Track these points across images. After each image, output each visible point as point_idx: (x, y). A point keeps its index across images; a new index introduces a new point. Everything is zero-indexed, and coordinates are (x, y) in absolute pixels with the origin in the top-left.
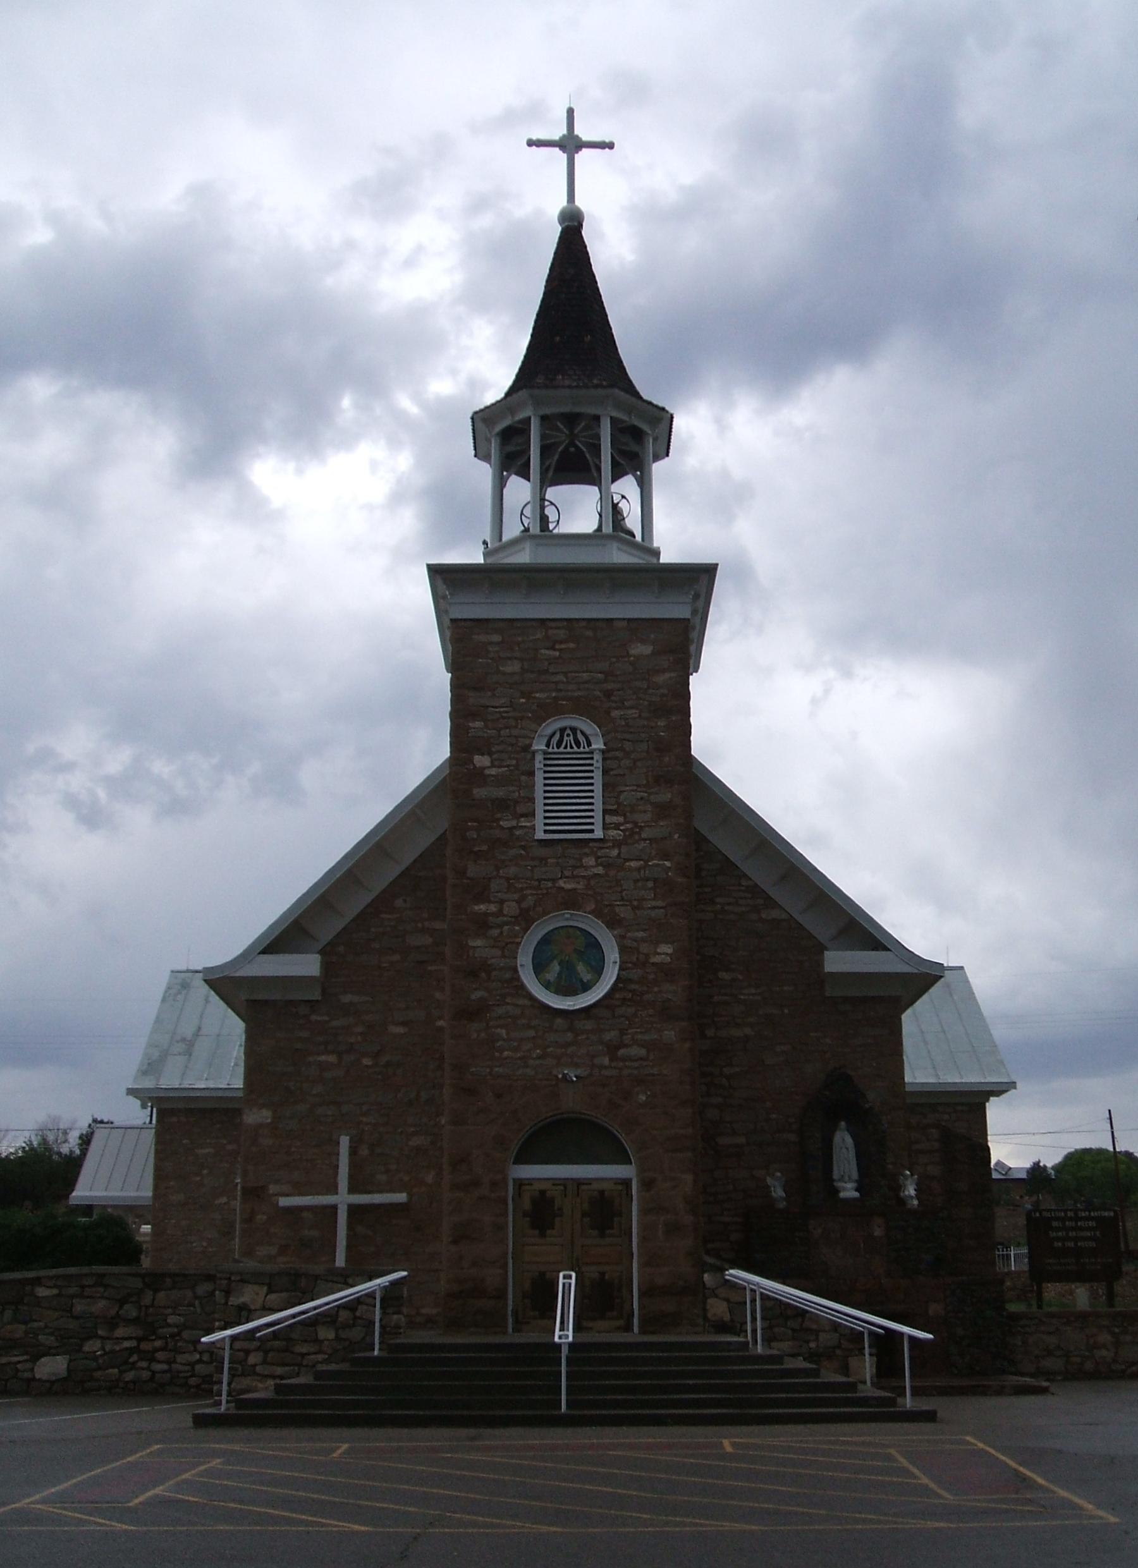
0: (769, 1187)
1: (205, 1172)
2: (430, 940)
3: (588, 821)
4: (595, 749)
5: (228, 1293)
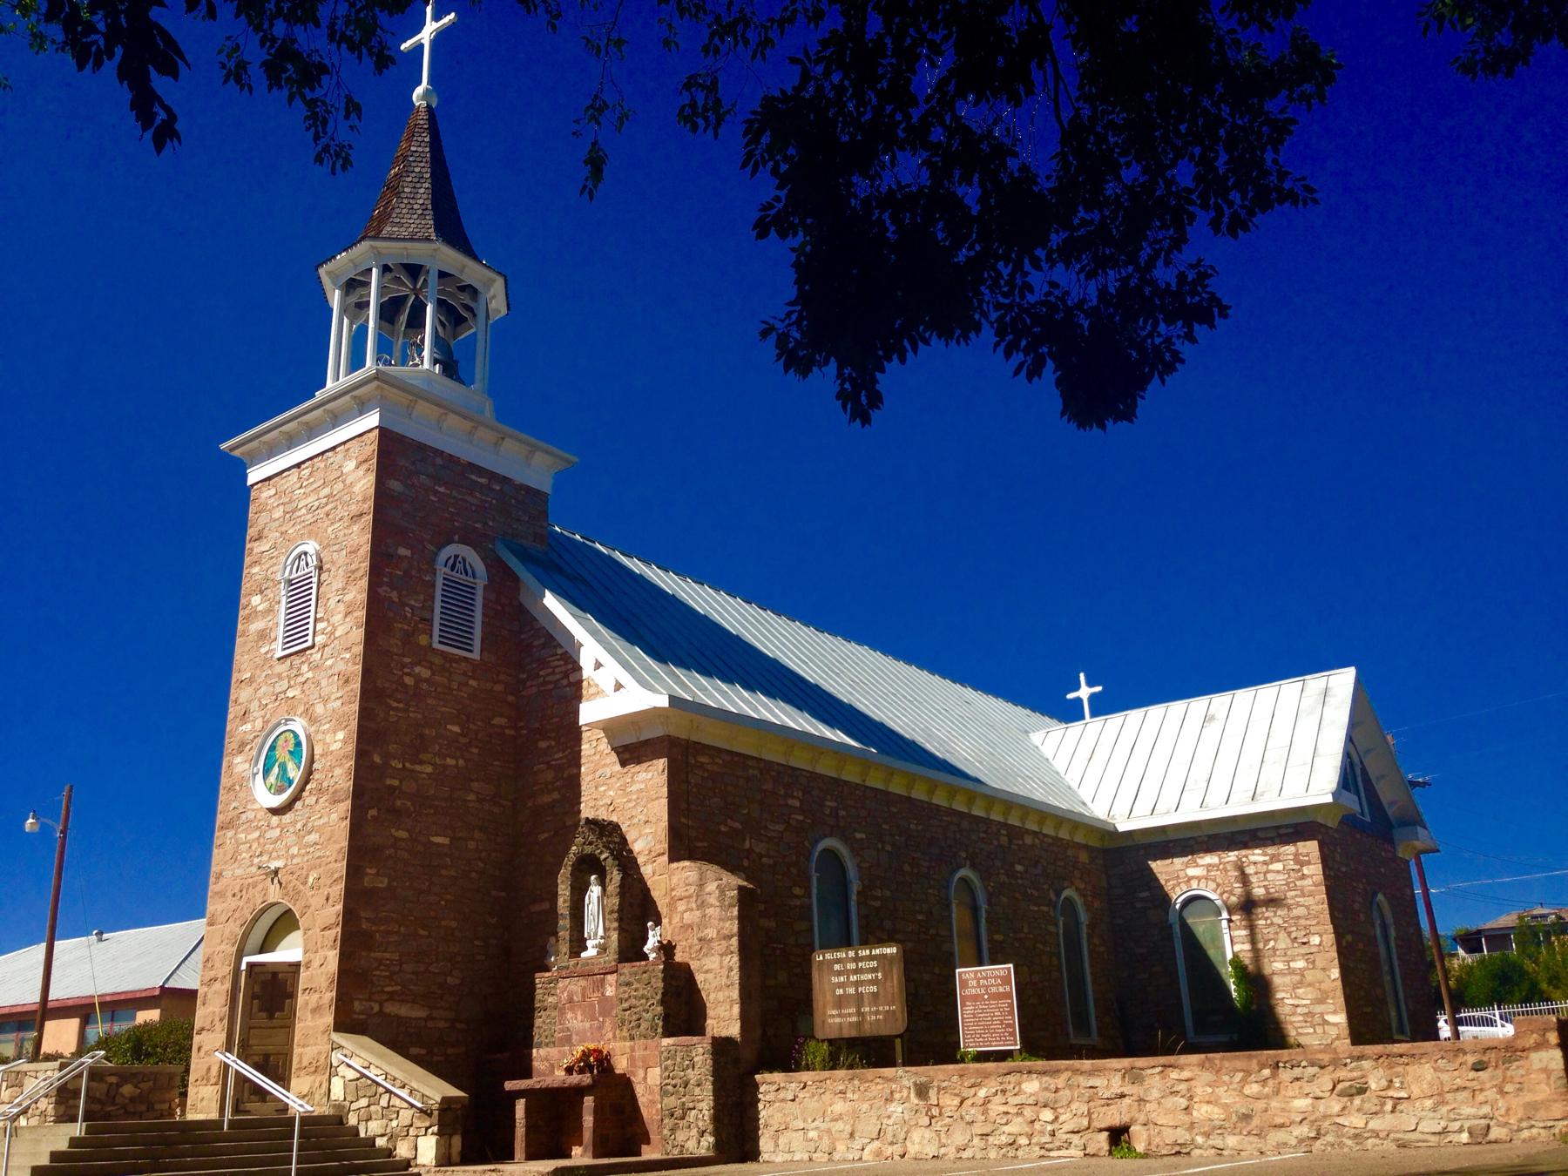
3: (468, 641)
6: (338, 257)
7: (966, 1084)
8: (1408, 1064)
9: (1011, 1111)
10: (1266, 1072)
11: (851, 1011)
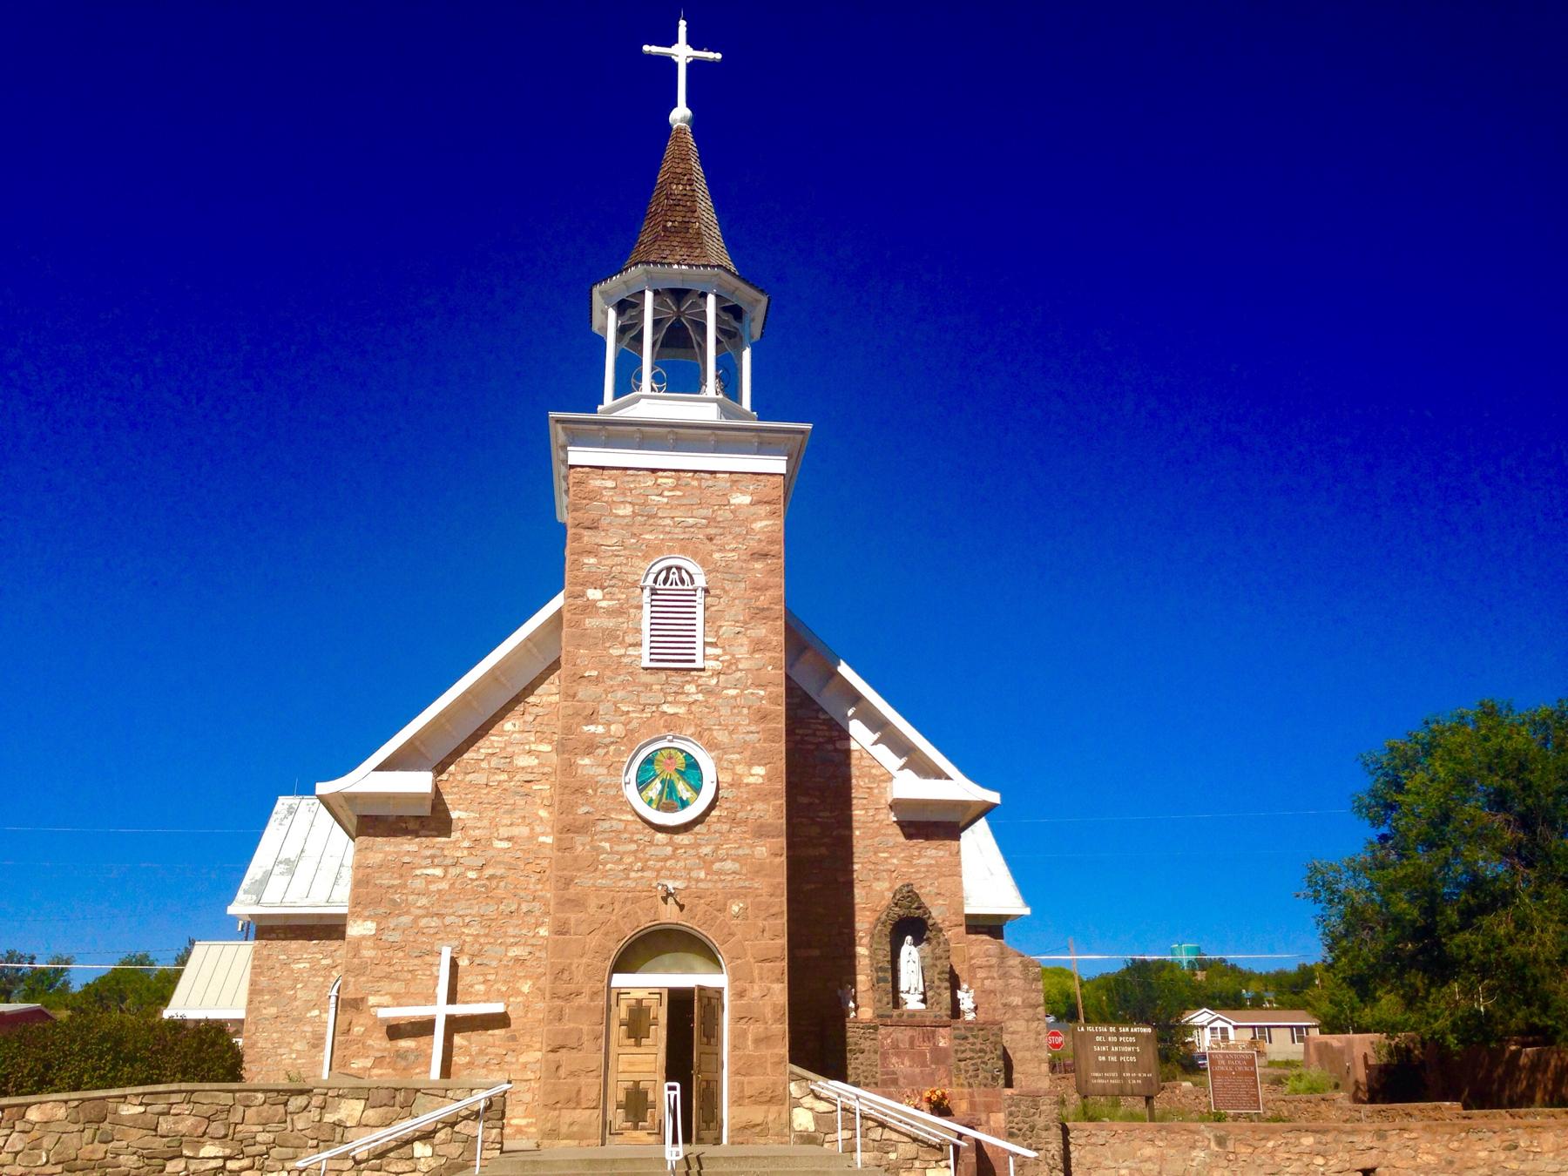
2: (536, 762)
6: (614, 278)
7: (1257, 1137)
8: (1540, 1132)
9: (1293, 1157)
10: (1463, 1135)
11: (1113, 1075)
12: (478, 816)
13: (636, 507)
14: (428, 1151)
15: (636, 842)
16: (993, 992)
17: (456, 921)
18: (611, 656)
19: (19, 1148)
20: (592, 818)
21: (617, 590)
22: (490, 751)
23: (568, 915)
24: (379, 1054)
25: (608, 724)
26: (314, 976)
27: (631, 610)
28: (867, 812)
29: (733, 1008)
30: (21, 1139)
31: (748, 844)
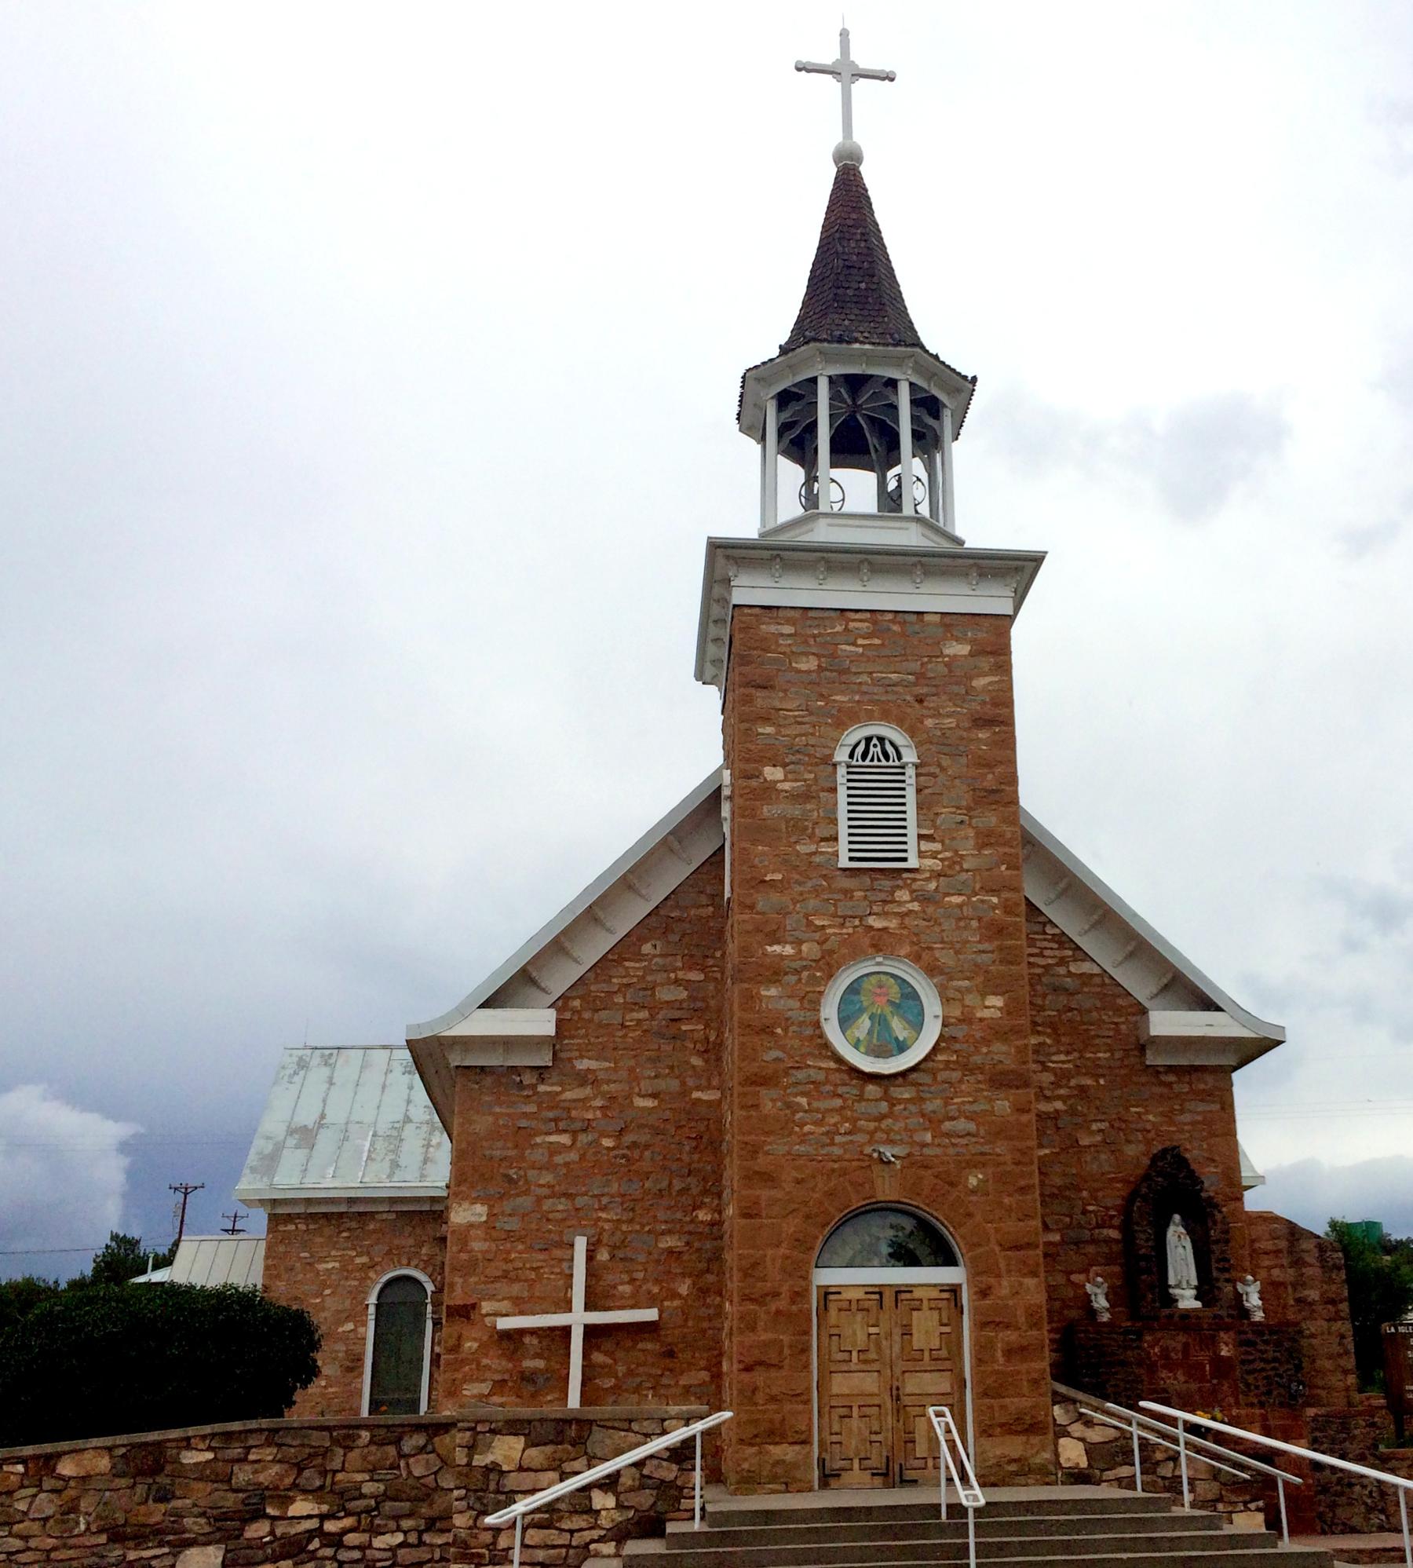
0: (1088, 1296)
1: (328, 1292)
2: (685, 994)
4: (907, 764)
5: (472, 1448)
12: (612, 1065)
13: (823, 660)
14: (610, 1501)
15: (840, 1096)
16: (1282, 1284)
17: (590, 1202)
18: (798, 854)
19: (49, 1512)
20: (782, 1066)
21: (802, 768)
22: (625, 981)
23: (758, 1192)
24: (498, 1377)
25: (798, 943)
26: (347, 1278)
27: (822, 794)
28: (1112, 1054)
29: (976, 1311)
30: (51, 1501)
31: (986, 1097)
